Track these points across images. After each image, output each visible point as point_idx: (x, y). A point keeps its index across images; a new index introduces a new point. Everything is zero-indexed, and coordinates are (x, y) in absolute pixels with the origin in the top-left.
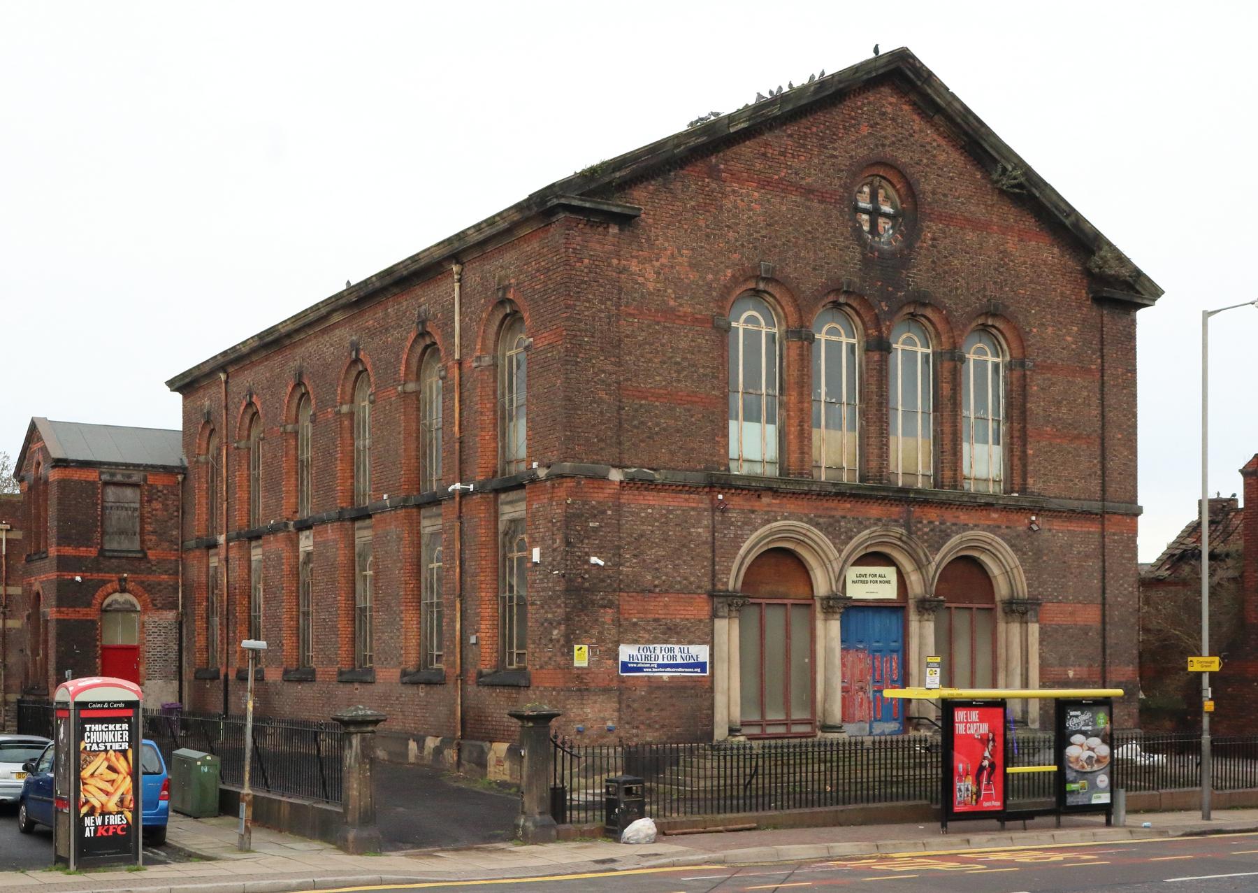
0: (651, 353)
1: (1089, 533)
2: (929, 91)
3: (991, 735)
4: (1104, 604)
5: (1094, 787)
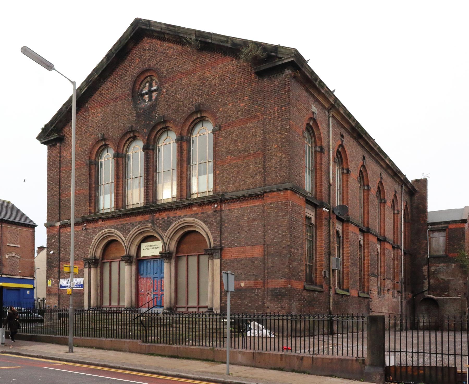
1: (255, 206)
2: (153, 28)
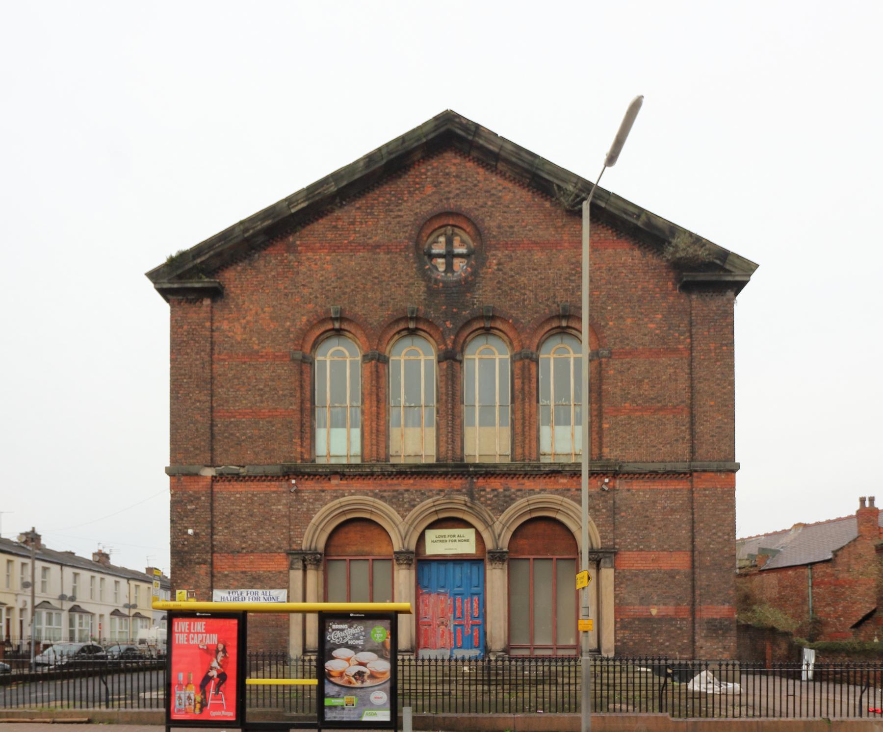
0: (239, 384)
1: (676, 490)
2: (481, 142)
3: (221, 647)
4: (693, 551)
5: (365, 703)
